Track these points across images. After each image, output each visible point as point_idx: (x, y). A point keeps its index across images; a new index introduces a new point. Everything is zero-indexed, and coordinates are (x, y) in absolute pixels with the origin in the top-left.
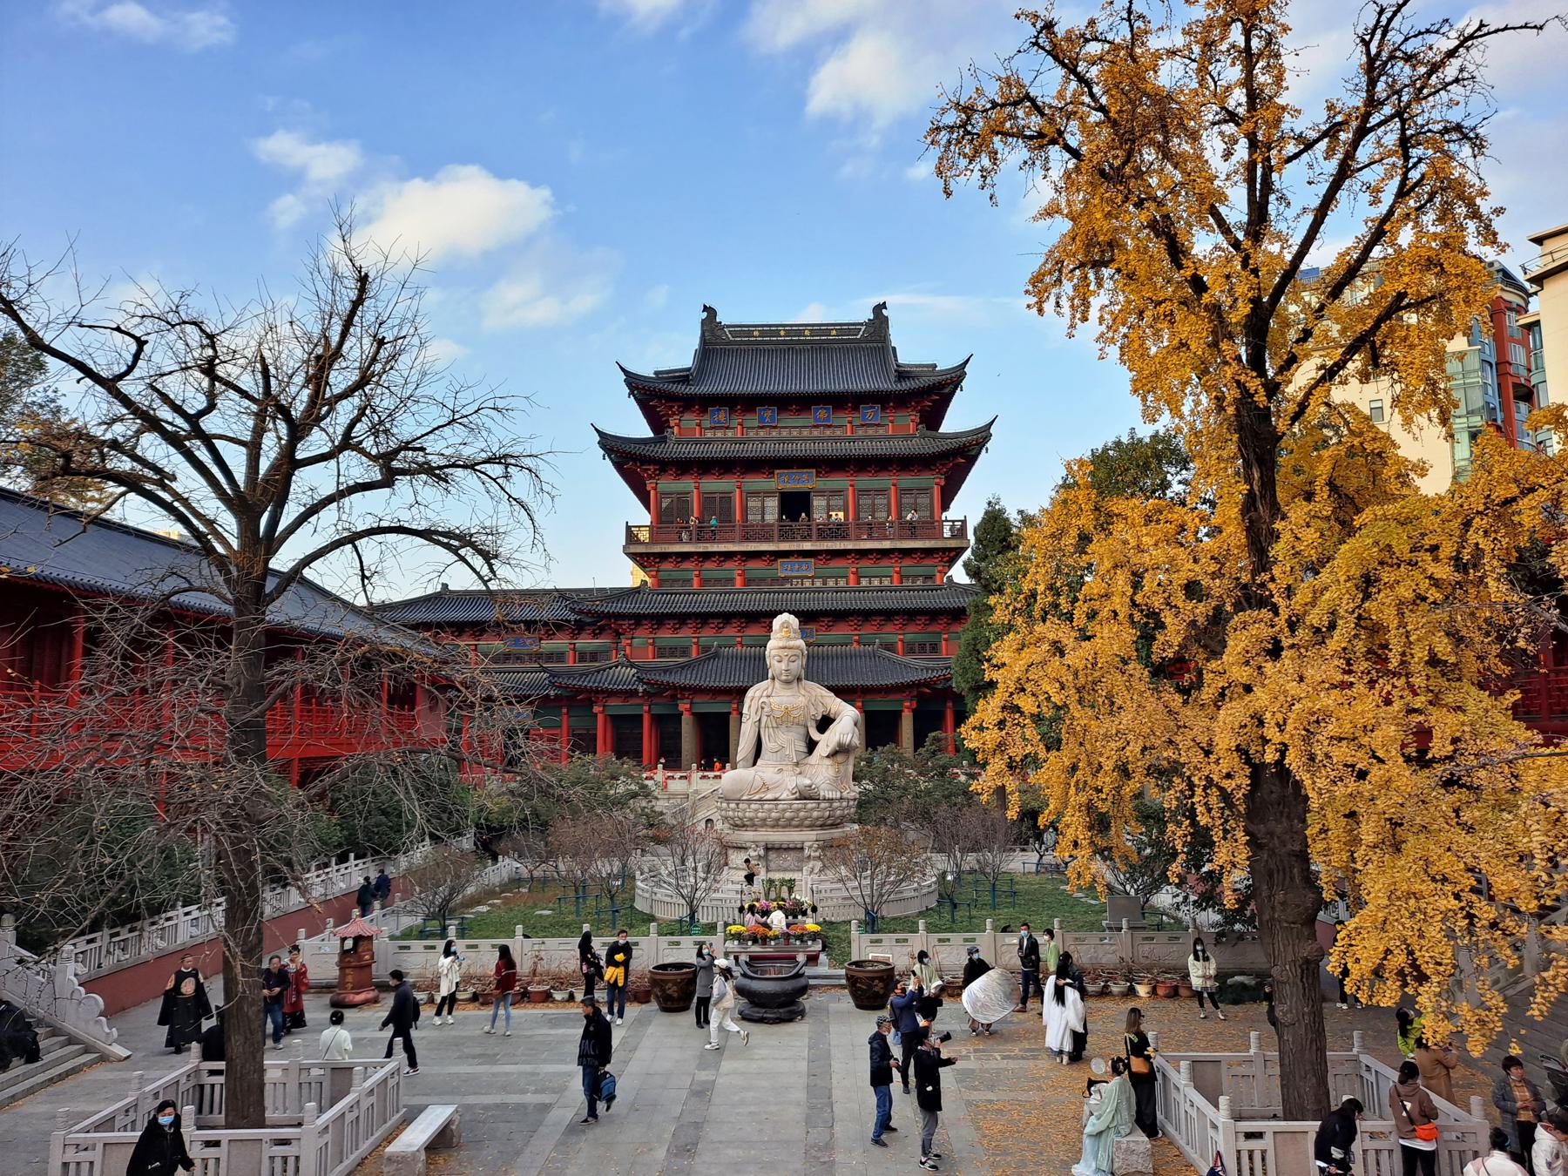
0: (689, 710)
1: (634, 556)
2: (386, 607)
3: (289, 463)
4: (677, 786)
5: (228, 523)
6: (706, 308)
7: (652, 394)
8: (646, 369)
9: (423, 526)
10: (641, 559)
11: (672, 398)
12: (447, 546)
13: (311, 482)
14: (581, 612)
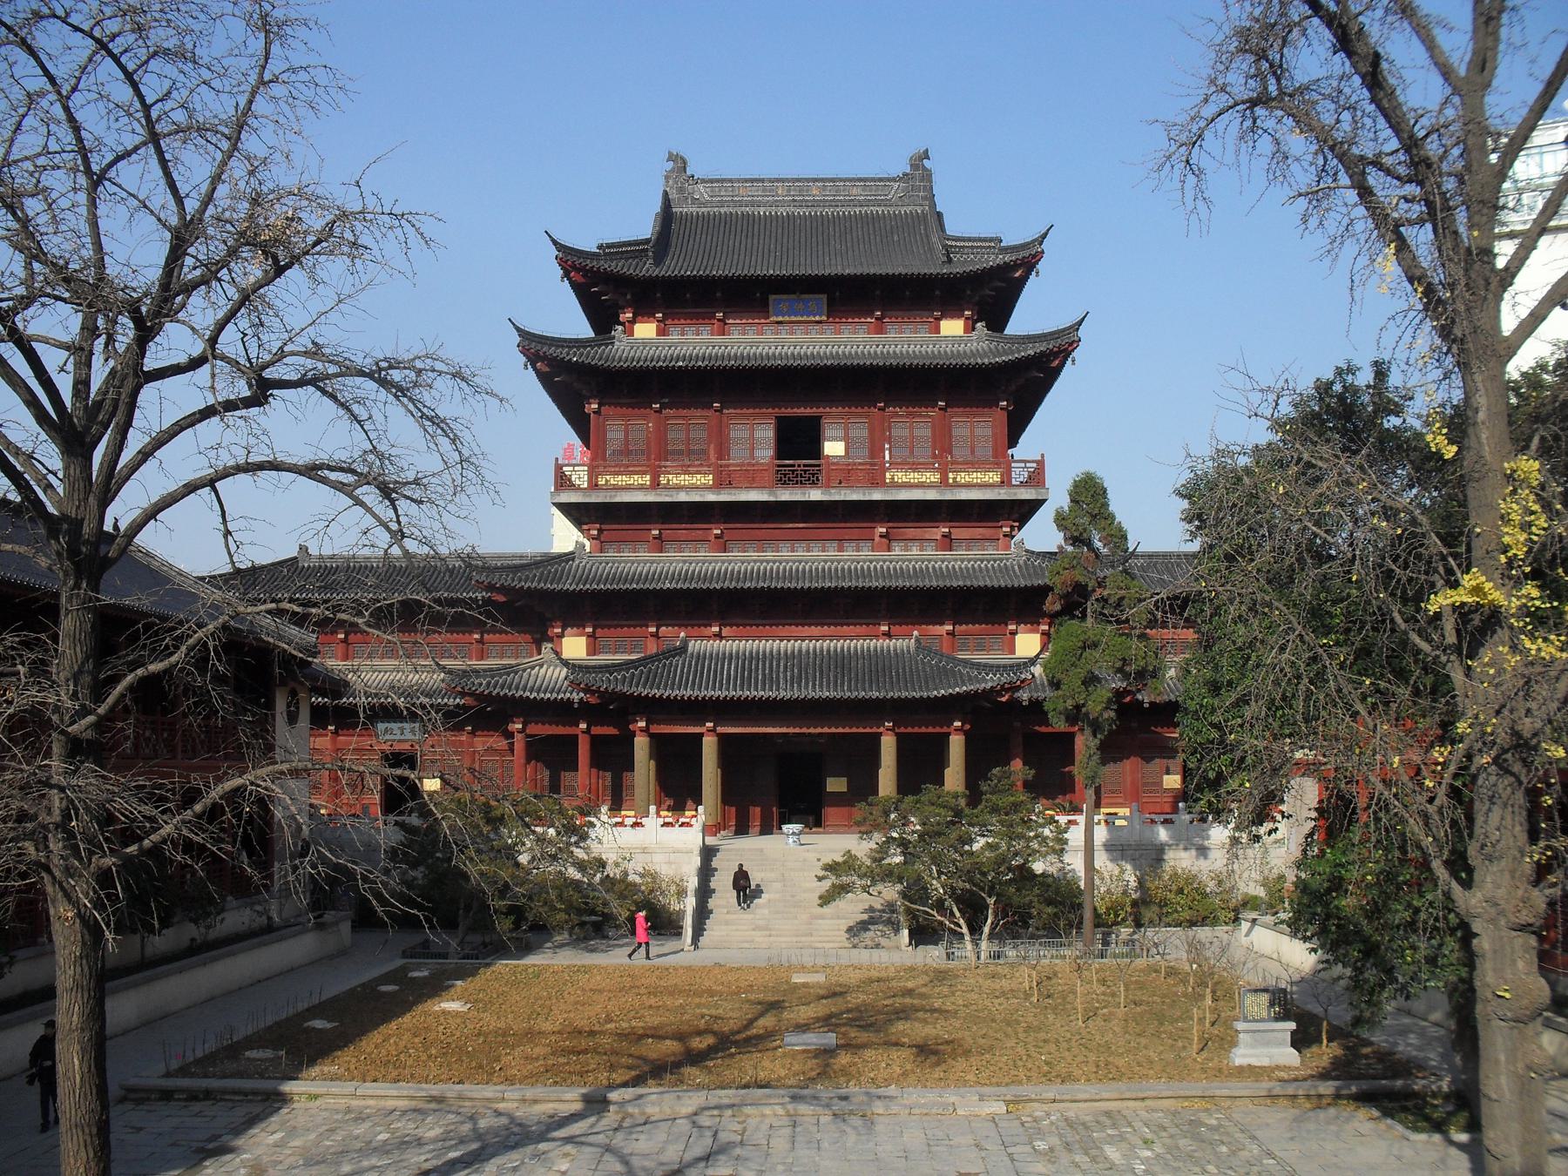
0: (646, 730)
1: (568, 510)
2: (255, 570)
3: (134, 376)
4: (627, 837)
5: (50, 456)
6: (672, 157)
7: (603, 284)
8: (587, 241)
9: (303, 456)
10: (577, 514)
11: (619, 282)
12: (339, 487)
13: (157, 406)
14: (491, 587)
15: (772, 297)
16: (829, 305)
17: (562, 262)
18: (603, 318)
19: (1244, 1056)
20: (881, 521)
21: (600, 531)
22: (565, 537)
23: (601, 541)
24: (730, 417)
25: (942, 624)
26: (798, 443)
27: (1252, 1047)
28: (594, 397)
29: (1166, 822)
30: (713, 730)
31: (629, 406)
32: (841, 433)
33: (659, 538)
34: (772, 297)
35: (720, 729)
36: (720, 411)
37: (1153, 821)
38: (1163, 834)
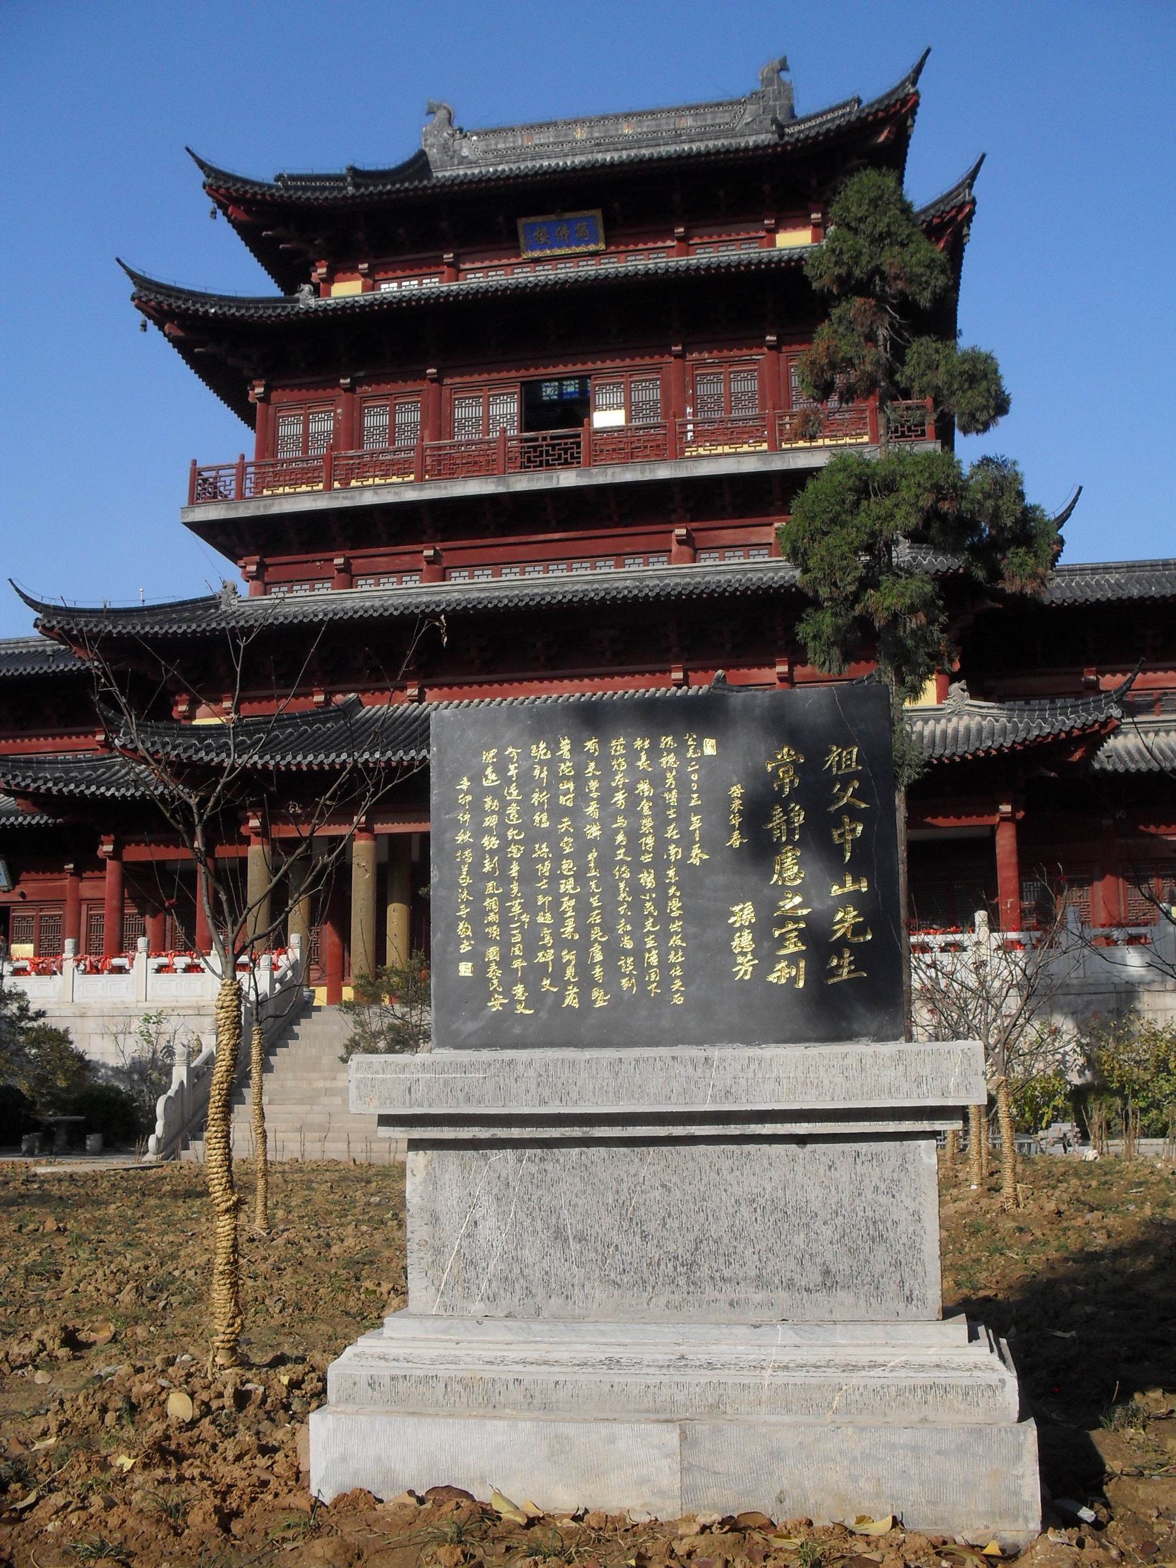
7: (283, 222)
15: (521, 222)
16: (607, 228)
17: (211, 190)
18: (289, 273)
19: (403, 1395)
20: (681, 521)
21: (262, 566)
22: (210, 575)
23: (261, 579)
24: (455, 389)
25: (772, 665)
26: (555, 420)
27: (524, 1296)
28: (260, 378)
29: (1133, 940)
30: (367, 829)
31: (315, 386)
32: (619, 397)
33: (346, 569)
34: (521, 222)
35: (379, 828)
36: (437, 380)
37: (1110, 941)
38: (1134, 962)
